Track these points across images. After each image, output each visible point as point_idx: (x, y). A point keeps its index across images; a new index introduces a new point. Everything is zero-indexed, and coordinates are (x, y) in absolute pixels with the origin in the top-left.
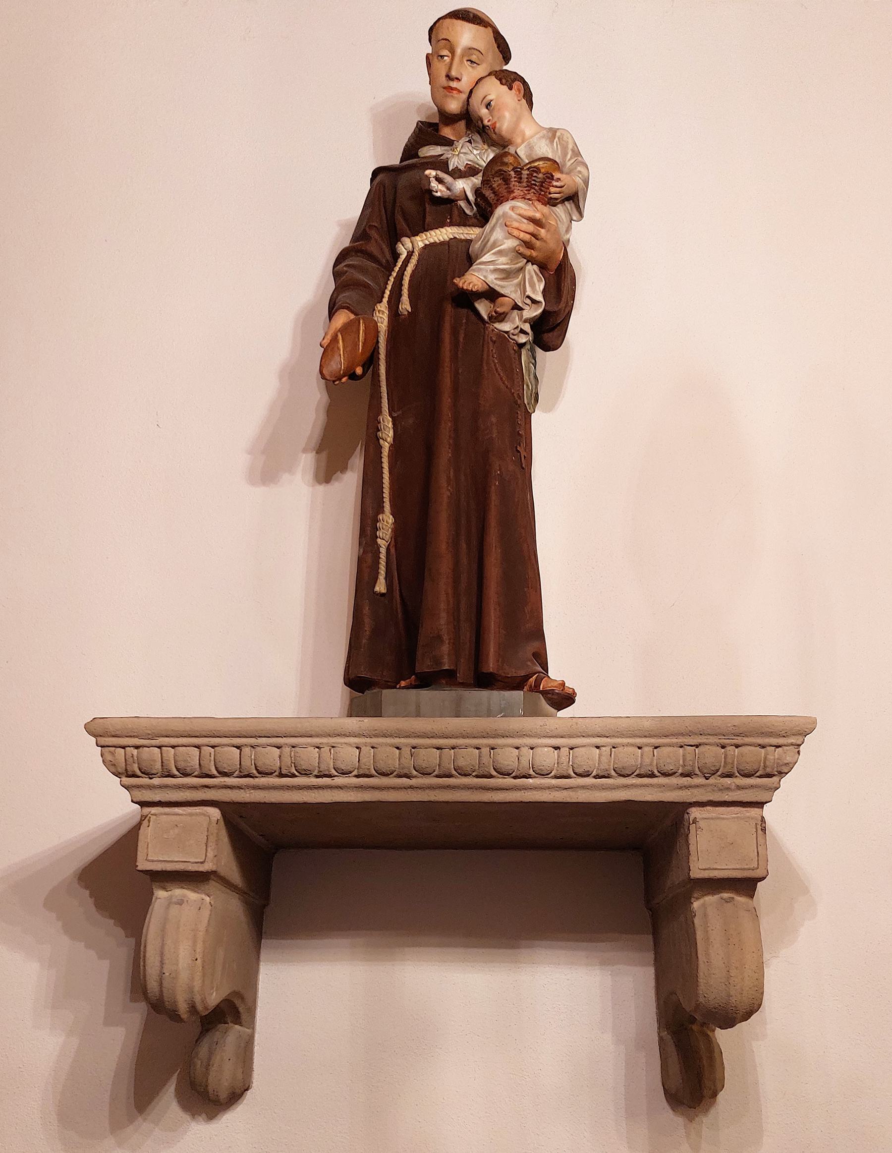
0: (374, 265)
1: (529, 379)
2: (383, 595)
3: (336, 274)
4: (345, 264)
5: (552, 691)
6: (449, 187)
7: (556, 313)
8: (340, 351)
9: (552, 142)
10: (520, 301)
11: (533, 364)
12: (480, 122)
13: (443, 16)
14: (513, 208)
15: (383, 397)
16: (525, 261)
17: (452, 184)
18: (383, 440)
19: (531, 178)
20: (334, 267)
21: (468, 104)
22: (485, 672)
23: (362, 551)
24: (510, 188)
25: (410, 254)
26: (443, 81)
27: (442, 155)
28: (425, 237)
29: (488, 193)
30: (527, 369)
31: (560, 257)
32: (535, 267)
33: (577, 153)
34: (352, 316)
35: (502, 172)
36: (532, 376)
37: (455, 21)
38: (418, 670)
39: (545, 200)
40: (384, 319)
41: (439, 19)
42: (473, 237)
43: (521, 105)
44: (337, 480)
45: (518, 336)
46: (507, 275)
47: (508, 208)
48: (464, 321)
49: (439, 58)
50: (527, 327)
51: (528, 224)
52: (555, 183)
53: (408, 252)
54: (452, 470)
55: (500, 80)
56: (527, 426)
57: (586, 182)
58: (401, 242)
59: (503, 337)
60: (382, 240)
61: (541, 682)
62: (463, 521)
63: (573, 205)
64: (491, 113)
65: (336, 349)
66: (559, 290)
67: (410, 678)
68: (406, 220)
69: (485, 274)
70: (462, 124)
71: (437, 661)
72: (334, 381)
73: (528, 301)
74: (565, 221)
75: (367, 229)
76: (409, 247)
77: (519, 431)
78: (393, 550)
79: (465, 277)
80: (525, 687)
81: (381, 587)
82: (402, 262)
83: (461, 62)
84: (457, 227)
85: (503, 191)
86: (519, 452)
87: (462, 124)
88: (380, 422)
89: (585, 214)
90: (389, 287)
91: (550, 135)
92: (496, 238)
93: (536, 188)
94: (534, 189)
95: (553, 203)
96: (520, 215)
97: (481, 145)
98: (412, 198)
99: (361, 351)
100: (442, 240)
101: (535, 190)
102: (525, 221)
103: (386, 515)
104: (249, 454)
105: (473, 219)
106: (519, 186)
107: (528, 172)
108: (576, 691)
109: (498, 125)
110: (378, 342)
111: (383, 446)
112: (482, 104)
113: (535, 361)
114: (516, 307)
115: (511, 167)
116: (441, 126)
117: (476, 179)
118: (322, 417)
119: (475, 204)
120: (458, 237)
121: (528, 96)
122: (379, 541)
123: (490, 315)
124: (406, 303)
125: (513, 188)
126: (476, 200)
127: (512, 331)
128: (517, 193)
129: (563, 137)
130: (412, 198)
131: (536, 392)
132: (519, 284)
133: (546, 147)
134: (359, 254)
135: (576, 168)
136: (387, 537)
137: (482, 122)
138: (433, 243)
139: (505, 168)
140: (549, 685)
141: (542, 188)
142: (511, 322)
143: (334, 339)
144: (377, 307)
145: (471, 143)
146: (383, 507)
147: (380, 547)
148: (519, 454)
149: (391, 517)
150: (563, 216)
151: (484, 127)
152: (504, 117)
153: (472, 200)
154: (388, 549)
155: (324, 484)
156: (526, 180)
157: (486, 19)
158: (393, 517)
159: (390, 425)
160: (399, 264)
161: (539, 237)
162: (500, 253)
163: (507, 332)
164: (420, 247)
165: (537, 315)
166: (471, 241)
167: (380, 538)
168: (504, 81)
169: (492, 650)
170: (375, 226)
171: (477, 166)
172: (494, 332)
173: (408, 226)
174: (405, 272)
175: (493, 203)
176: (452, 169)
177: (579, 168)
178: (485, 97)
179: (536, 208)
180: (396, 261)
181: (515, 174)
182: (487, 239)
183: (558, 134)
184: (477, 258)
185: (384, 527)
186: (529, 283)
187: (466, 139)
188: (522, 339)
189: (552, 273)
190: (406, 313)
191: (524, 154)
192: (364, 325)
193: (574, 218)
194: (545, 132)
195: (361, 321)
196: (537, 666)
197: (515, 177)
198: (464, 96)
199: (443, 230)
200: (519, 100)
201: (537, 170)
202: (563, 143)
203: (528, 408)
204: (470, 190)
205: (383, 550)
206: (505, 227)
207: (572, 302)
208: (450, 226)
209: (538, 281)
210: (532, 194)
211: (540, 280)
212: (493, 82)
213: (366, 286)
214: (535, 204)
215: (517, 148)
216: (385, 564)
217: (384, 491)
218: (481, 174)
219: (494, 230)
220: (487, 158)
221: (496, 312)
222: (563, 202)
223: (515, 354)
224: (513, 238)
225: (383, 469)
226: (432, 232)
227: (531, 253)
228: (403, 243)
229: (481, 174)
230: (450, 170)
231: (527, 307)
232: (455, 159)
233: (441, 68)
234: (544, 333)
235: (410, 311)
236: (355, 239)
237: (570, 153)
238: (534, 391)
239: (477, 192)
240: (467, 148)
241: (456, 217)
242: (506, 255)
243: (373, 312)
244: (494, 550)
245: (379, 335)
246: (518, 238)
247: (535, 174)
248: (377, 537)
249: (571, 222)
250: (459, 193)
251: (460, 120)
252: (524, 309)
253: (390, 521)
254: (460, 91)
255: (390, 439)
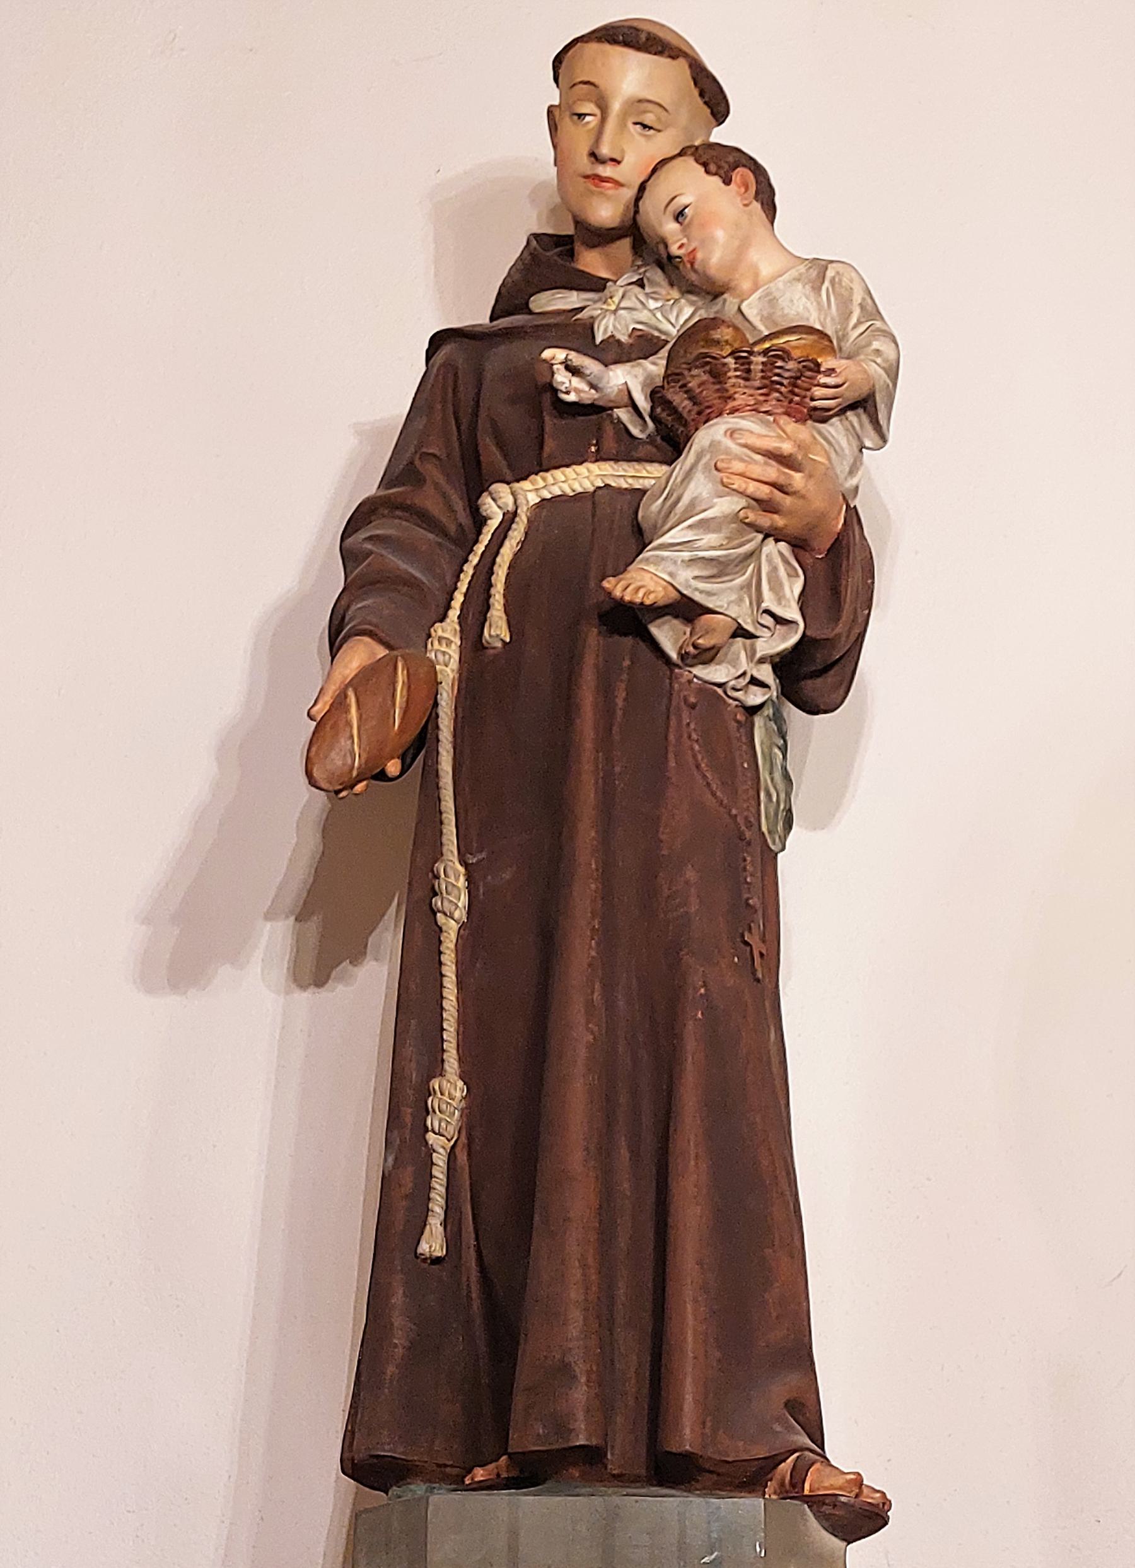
0: (431, 536)
1: (772, 779)
2: (437, 1261)
3: (349, 557)
4: (368, 534)
5: (833, 1498)
6: (595, 382)
7: (829, 643)
8: (351, 727)
9: (817, 289)
10: (749, 621)
11: (780, 748)
12: (661, 247)
13: (583, 36)
14: (732, 433)
15: (446, 821)
16: (760, 536)
17: (600, 379)
18: (445, 914)
19: (771, 370)
20: (343, 538)
21: (637, 212)
22: (674, 1450)
23: (390, 1160)
24: (727, 391)
25: (510, 518)
26: (584, 163)
27: (582, 309)
28: (541, 484)
29: (680, 400)
30: (768, 758)
31: (837, 526)
32: (783, 546)
33: (871, 312)
34: (381, 652)
35: (708, 359)
36: (778, 775)
37: (607, 47)
38: (510, 1450)
39: (801, 412)
40: (450, 657)
41: (576, 41)
42: (648, 483)
43: (750, 214)
44: (340, 979)
45: (746, 692)
46: (721, 569)
47: (722, 432)
48: (627, 663)
49: (576, 118)
50: (766, 673)
51: (766, 463)
52: (823, 380)
53: (504, 514)
54: (597, 986)
55: (705, 165)
56: (770, 869)
57: (893, 372)
58: (490, 494)
59: (712, 694)
60: (449, 481)
61: (806, 1475)
62: (623, 1099)
63: (864, 418)
64: (686, 230)
65: (341, 724)
66: (836, 593)
67: (497, 1460)
68: (501, 445)
69: (671, 568)
70: (626, 244)
71: (562, 1427)
72: (337, 792)
73: (768, 621)
74: (847, 451)
75: (417, 462)
76: (506, 504)
77: (748, 899)
78: (462, 1157)
79: (627, 575)
80: (769, 1483)
81: (433, 1243)
82: (493, 534)
83: (622, 125)
84: (612, 463)
85: (709, 394)
86: (747, 944)
87: (626, 244)
88: (437, 877)
89: (891, 437)
90: (463, 586)
91: (814, 273)
92: (694, 495)
93: (783, 389)
94: (778, 391)
95: (821, 416)
96: (746, 446)
97: (664, 290)
98: (513, 400)
99: (399, 726)
100: (580, 490)
101: (781, 393)
102: (758, 457)
103: (449, 1081)
104: (143, 923)
105: (649, 447)
106: (746, 387)
107: (765, 359)
108: (889, 1497)
109: (699, 255)
110: (436, 704)
111: (444, 928)
112: (668, 213)
113: (785, 742)
114: (740, 632)
115: (728, 350)
116: (578, 247)
117: (654, 364)
118: (313, 842)
119: (651, 416)
120: (613, 484)
121: (766, 197)
122: (431, 1137)
123: (683, 652)
124: (500, 623)
125: (732, 391)
126: (653, 408)
127: (732, 683)
128: (740, 400)
129: (840, 280)
130: (513, 400)
131: (787, 808)
132: (748, 585)
133: (804, 299)
134: (398, 513)
135: (869, 344)
136: (451, 1129)
137: (666, 246)
138: (559, 496)
139: (715, 351)
140: (826, 1484)
141: (796, 390)
142: (729, 663)
143: (340, 703)
144: (435, 631)
145: (642, 286)
146: (443, 1061)
147: (434, 1151)
148: (748, 949)
149: (460, 1084)
150: (844, 443)
151: (670, 258)
152: (713, 239)
153: (645, 410)
154: (452, 1155)
155: (312, 989)
156: (760, 375)
157: (675, 42)
158: (465, 1083)
159: (462, 883)
160: (485, 538)
161: (791, 490)
162: (705, 525)
163: (720, 685)
164: (532, 503)
165: (786, 649)
166: (643, 492)
167: (434, 1132)
168: (713, 168)
169: (689, 1398)
170: (434, 456)
171: (656, 334)
172: (692, 685)
173: (505, 456)
174: (498, 560)
175: (689, 419)
176: (602, 342)
177: (876, 345)
178: (675, 197)
179: (784, 431)
180: (479, 533)
181: (736, 363)
182: (675, 496)
183: (830, 273)
184: (658, 531)
185: (444, 1107)
186: (769, 582)
187: (631, 277)
188: (755, 697)
189: (820, 557)
190: (499, 645)
191: (758, 314)
192: (405, 672)
193: (868, 443)
194: (802, 268)
195: (400, 665)
196: (798, 1433)
197: (736, 370)
198: (629, 193)
199: (582, 469)
200: (746, 205)
201: (784, 354)
202: (843, 291)
203: (769, 841)
204: (640, 388)
205: (440, 1160)
206: (715, 472)
207: (867, 612)
208: (597, 461)
209: (789, 575)
210: (774, 402)
211: (792, 575)
212: (689, 171)
213: (410, 583)
214: (781, 422)
215: (742, 301)
216: (444, 1190)
217: (445, 1026)
218: (664, 352)
219: (692, 479)
220: (677, 317)
221: (695, 646)
222: (842, 412)
223: (738, 730)
224: (732, 495)
225: (443, 966)
226: (558, 474)
227: (771, 519)
228: (494, 495)
229: (664, 352)
230: (598, 340)
231: (766, 633)
232: (608, 320)
233: (579, 139)
234: (805, 678)
235: (508, 640)
236: (387, 481)
237: (856, 314)
238: (782, 807)
239: (656, 395)
240: (634, 299)
241: (610, 444)
242: (717, 530)
243: (427, 639)
244: (692, 1163)
245: (440, 690)
246: (742, 494)
247: (779, 364)
248: (426, 1130)
249: (861, 451)
250: (617, 395)
251: (620, 237)
252: (757, 637)
253: (458, 1094)
254: (618, 184)
255: (460, 914)
